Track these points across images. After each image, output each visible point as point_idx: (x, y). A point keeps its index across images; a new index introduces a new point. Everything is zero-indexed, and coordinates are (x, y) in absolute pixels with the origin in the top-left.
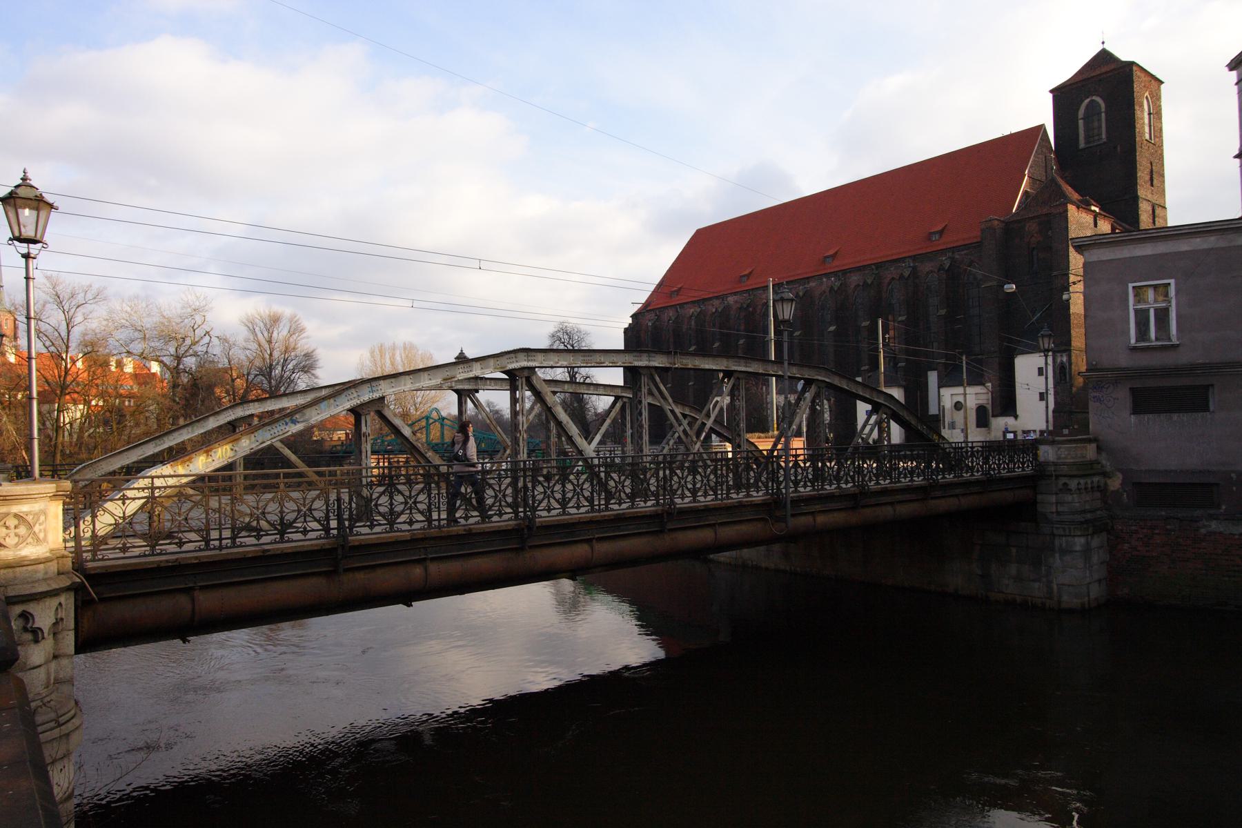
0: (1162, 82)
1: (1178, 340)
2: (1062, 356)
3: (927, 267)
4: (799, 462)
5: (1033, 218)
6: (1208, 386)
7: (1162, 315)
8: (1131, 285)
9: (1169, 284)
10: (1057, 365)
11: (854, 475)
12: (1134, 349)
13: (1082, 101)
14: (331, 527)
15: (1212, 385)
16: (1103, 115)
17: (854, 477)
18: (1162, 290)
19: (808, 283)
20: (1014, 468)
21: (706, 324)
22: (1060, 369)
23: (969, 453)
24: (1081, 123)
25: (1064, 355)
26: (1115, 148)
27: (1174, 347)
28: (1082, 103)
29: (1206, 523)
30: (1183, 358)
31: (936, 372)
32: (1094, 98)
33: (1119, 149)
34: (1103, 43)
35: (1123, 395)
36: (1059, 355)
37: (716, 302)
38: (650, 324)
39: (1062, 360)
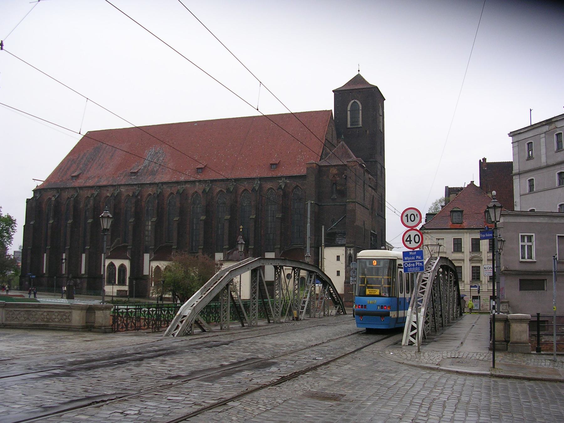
0: (385, 100)
1: (536, 259)
2: (350, 250)
3: (268, 185)
4: (120, 313)
5: (334, 166)
6: (544, 280)
7: (530, 247)
8: (520, 234)
9: (533, 235)
10: (347, 255)
11: (136, 323)
12: (521, 262)
13: (350, 101)
14: (536, 318)
15: (546, 280)
16: (361, 112)
17: (136, 324)
18: (530, 238)
19: (185, 185)
20: (161, 324)
21: (101, 203)
22: (349, 257)
23: (146, 312)
24: (349, 112)
25: (352, 249)
26: (366, 131)
27: (535, 262)
28: (350, 102)
29: (544, 337)
30: (539, 267)
31: (274, 253)
32: (356, 101)
33: (368, 132)
34: (359, 71)
35: (515, 283)
36: (349, 249)
37: (111, 189)
38: (53, 199)
39: (350, 252)
